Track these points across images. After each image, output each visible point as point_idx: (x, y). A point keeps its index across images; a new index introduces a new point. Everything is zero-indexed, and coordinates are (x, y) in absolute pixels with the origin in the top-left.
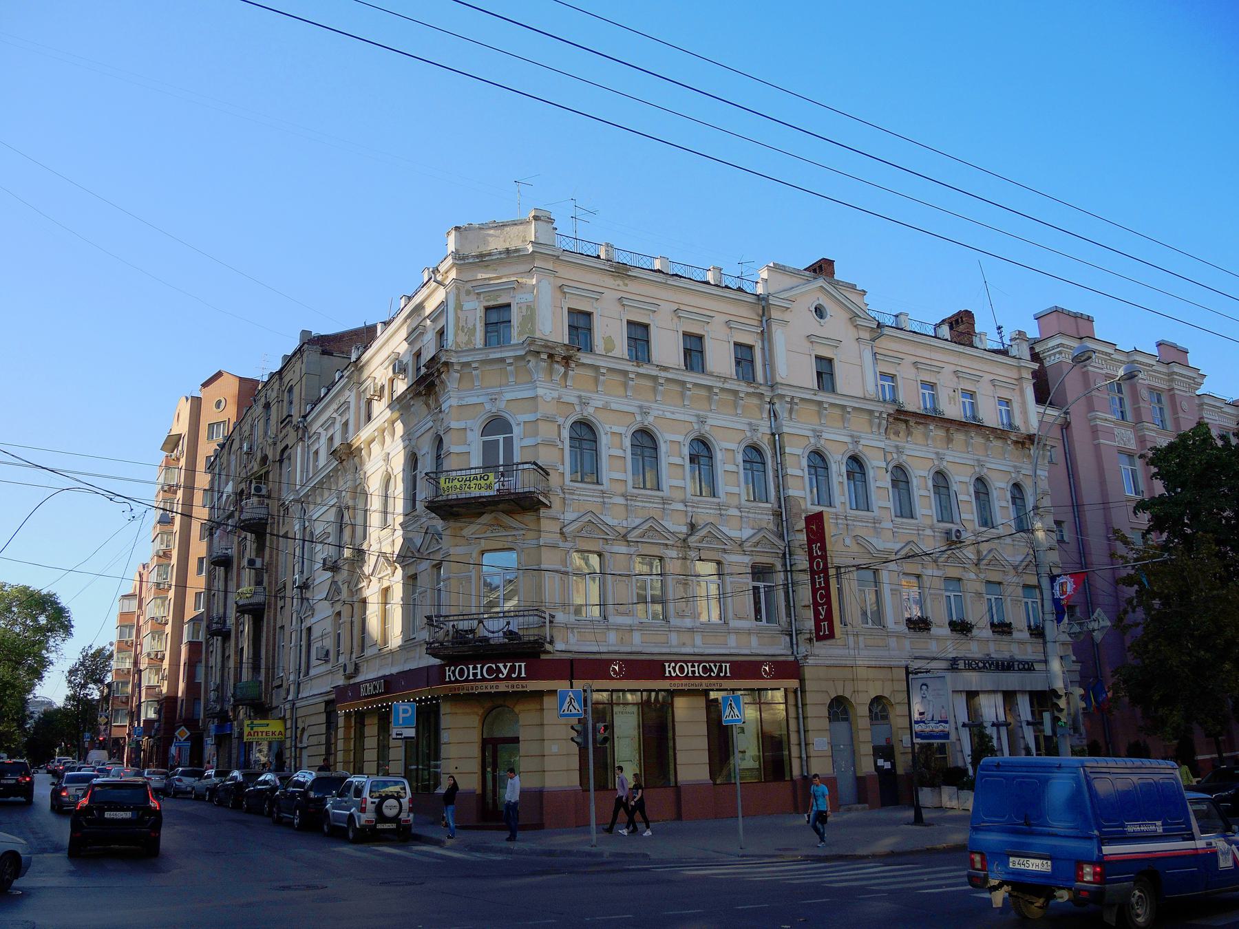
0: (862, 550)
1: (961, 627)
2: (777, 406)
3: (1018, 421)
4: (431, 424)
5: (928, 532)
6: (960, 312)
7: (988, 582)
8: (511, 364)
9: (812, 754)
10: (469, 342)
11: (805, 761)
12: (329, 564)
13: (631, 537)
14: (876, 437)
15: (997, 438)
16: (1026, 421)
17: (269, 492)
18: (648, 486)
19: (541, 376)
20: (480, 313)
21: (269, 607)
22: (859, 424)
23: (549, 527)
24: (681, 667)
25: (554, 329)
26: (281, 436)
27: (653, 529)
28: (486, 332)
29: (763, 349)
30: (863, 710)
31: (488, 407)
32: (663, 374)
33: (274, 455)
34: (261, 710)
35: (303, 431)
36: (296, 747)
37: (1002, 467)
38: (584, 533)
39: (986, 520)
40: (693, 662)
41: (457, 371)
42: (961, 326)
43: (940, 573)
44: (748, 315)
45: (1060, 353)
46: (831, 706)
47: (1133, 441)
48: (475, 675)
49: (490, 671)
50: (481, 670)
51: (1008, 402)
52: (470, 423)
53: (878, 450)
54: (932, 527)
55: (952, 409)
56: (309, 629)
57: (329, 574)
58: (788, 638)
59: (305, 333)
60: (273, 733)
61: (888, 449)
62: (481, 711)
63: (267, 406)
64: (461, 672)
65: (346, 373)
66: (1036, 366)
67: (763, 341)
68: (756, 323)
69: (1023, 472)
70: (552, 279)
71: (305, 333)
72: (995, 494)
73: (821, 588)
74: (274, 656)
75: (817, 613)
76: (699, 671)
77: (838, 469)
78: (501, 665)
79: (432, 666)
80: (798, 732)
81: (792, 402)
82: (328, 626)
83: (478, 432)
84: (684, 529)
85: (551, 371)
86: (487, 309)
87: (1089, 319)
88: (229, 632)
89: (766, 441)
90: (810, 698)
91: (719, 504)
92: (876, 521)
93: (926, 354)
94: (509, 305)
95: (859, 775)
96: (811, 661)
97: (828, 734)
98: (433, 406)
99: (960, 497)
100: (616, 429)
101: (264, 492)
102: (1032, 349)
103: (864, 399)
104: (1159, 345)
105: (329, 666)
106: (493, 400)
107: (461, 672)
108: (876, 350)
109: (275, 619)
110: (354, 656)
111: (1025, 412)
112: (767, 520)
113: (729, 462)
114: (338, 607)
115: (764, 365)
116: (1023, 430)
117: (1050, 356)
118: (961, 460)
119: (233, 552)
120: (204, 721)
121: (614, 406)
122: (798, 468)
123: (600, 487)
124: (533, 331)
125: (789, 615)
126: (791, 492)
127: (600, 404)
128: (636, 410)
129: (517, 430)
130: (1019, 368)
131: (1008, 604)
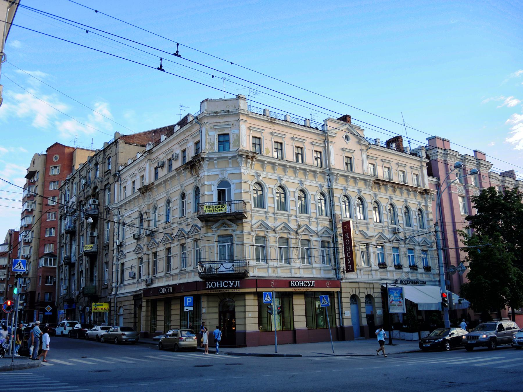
0: (362, 236)
1: (398, 267)
4: (193, 181)
5: (386, 228)
8: (230, 159)
9: (344, 317)
10: (212, 149)
13: (277, 230)
19: (243, 165)
20: (216, 137)
22: (361, 184)
24: (297, 283)
25: (246, 145)
26: (104, 179)
27: (286, 227)
28: (219, 145)
29: (325, 153)
30: (363, 300)
31: (220, 176)
32: (289, 164)
34: (96, 298)
36: (116, 315)
37: (414, 202)
38: (282, 231)
39: (409, 224)
40: (301, 281)
42: (395, 142)
43: (391, 245)
44: (319, 140)
46: (351, 298)
48: (219, 286)
49: (226, 284)
50: (222, 284)
52: (212, 182)
53: (368, 194)
54: (388, 227)
55: (397, 179)
56: (123, 264)
57: (135, 241)
60: (105, 309)
62: (219, 300)
64: (214, 285)
66: (428, 161)
72: (412, 213)
73: (349, 251)
74: (102, 275)
75: (347, 261)
76: (303, 284)
78: (230, 282)
79: (198, 281)
80: (339, 308)
81: (337, 176)
82: (135, 263)
83: (216, 187)
85: (246, 163)
86: (219, 135)
87: (448, 141)
89: (326, 191)
90: (343, 295)
94: (228, 134)
96: (344, 280)
98: (194, 174)
99: (399, 214)
100: (270, 186)
101: (97, 203)
102: (426, 153)
103: (363, 174)
105: (135, 280)
106: (223, 174)
107: (214, 285)
109: (102, 259)
110: (150, 276)
112: (327, 224)
114: (140, 256)
115: (326, 160)
118: (399, 200)
121: (270, 177)
123: (265, 210)
124: (239, 146)
125: (335, 262)
127: (264, 176)
130: (421, 162)
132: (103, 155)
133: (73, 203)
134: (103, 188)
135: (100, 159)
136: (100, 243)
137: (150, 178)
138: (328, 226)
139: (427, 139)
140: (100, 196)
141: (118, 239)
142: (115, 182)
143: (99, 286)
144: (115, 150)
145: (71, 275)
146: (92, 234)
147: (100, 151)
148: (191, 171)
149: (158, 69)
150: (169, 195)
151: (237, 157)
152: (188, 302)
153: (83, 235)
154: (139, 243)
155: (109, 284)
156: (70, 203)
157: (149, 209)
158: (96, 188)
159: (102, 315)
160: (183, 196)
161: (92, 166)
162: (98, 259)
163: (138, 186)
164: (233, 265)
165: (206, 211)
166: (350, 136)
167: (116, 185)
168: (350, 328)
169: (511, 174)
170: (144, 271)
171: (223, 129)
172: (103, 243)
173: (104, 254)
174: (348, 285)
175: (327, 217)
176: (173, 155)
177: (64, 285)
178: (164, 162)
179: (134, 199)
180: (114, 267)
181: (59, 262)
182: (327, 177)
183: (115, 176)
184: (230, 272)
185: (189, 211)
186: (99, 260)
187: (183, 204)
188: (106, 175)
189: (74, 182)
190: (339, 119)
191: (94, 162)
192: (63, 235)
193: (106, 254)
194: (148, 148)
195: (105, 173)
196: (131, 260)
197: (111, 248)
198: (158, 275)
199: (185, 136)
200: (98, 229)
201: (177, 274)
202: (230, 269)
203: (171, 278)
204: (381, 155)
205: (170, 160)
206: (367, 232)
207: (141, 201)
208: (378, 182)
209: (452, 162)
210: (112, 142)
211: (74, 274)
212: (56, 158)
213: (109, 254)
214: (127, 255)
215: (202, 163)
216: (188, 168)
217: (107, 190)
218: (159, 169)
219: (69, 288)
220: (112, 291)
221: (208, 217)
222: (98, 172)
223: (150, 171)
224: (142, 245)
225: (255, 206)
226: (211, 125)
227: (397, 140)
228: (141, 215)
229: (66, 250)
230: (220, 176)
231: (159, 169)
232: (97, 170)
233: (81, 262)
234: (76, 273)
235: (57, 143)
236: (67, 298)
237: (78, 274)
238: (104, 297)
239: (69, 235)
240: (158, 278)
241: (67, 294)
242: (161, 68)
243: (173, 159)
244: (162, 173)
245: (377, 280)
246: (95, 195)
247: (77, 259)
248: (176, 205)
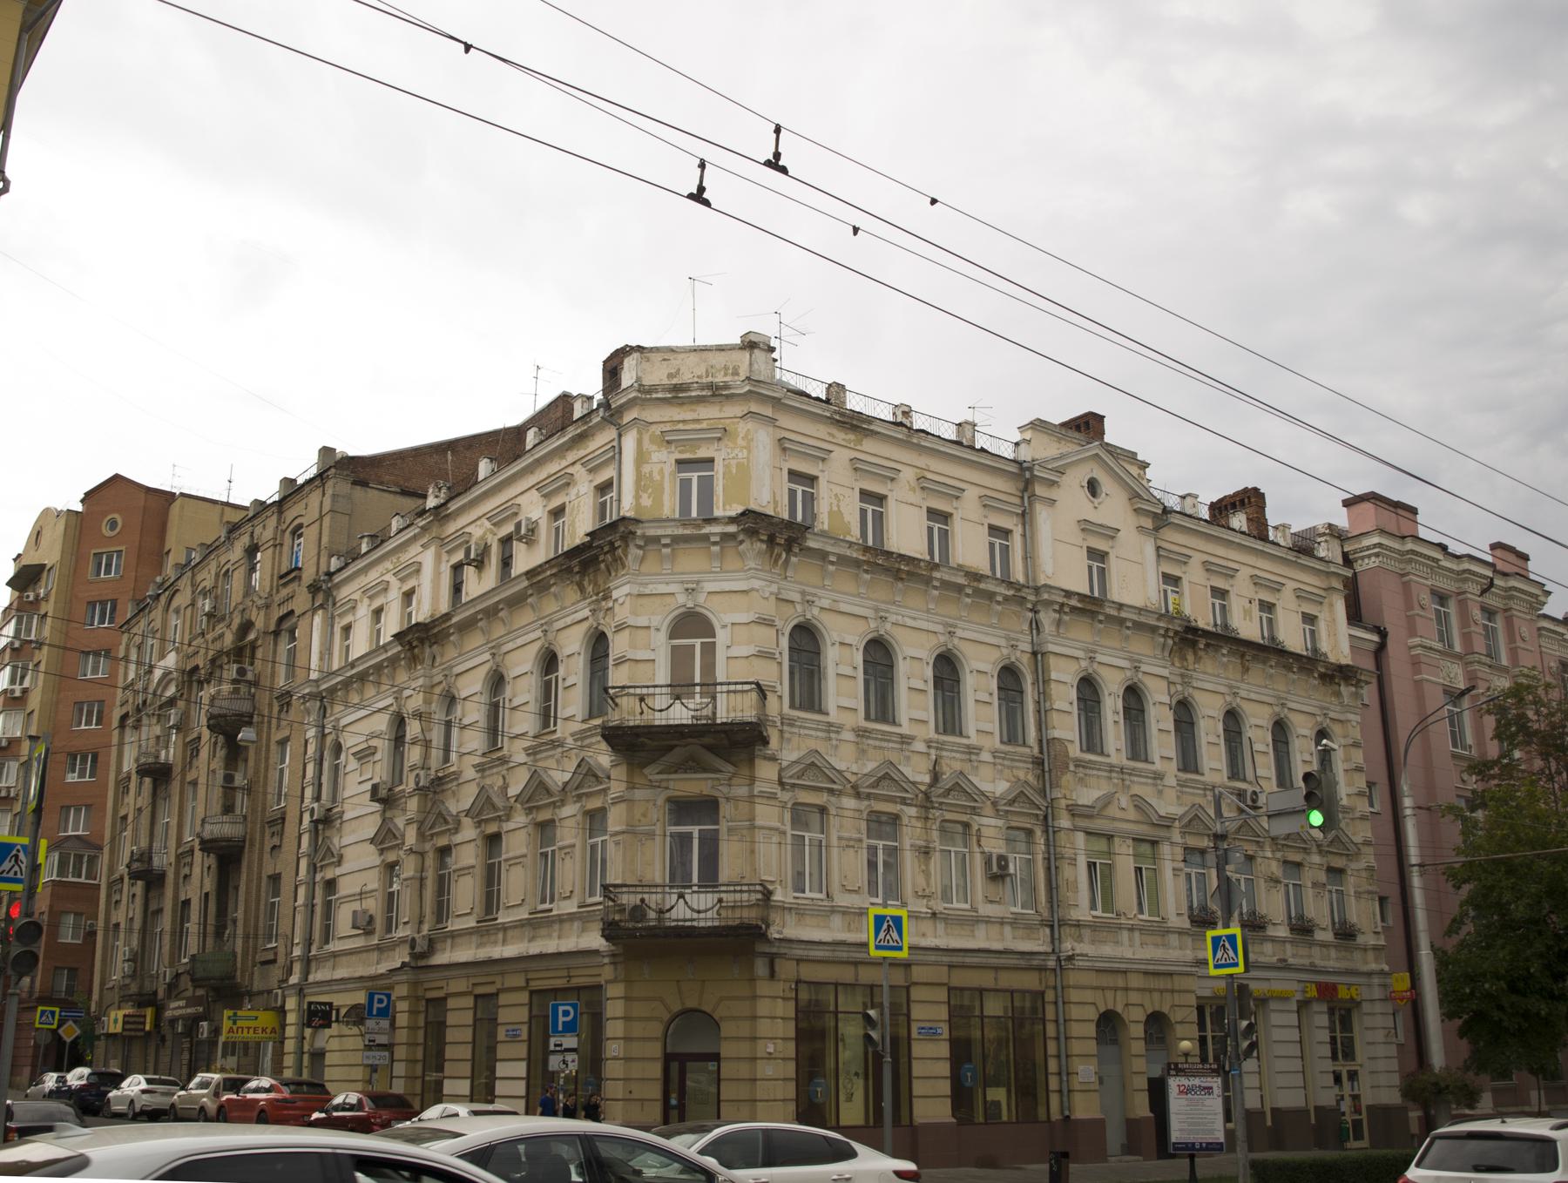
2: (1042, 615)
3: (1325, 646)
4: (586, 612)
6: (1246, 490)
7: (1285, 862)
11: (1066, 1093)
12: (383, 793)
14: (1161, 662)
15: (1301, 669)
16: (1335, 646)
18: (873, 716)
20: (670, 467)
21: (252, 845)
23: (766, 772)
26: (277, 599)
29: (1024, 535)
30: (1137, 1030)
33: (266, 625)
37: (1305, 706)
41: (639, 547)
45: (1377, 555)
51: (1006, 533)
55: (1248, 627)
58: (1048, 930)
59: (326, 452)
61: (1173, 678)
63: (252, 550)
65: (421, 522)
66: (1349, 573)
67: (1024, 525)
70: (771, 429)
71: (326, 452)
84: (927, 779)
88: (162, 876)
91: (968, 746)
92: (1158, 776)
94: (712, 460)
97: (1095, 1060)
98: (590, 589)
99: (1257, 747)
101: (250, 676)
104: (1347, 503)
108: (1160, 543)
111: (1333, 634)
116: (1332, 659)
117: (1363, 558)
118: (1260, 698)
119: (171, 754)
122: (1065, 697)
125: (1050, 900)
126: (1056, 734)
128: (796, 597)
129: (722, 637)
131: (1309, 893)
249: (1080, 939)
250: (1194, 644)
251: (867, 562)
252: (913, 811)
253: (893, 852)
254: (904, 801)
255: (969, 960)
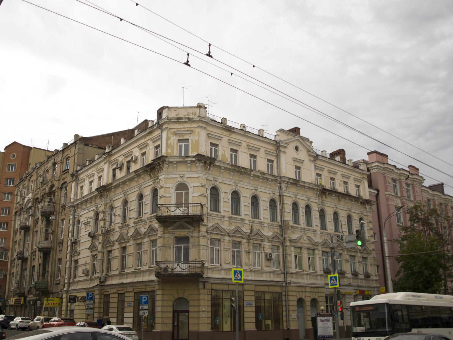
3: (362, 194)
4: (152, 183)
6: (340, 150)
8: (189, 163)
11: (288, 321)
12: (92, 235)
15: (355, 201)
17: (56, 201)
18: (234, 213)
20: (176, 141)
23: (203, 229)
26: (62, 178)
27: (238, 231)
30: (308, 304)
33: (58, 185)
35: (75, 176)
37: (356, 211)
41: (167, 164)
44: (272, 148)
45: (377, 168)
47: (400, 203)
55: (340, 189)
56: (76, 261)
57: (90, 239)
58: (283, 275)
59: (76, 136)
61: (319, 203)
63: (54, 164)
67: (277, 159)
68: (275, 152)
69: (364, 214)
77: (302, 211)
82: (89, 260)
84: (249, 231)
88: (27, 259)
91: (261, 222)
93: (333, 167)
94: (188, 140)
95: (307, 328)
97: (296, 312)
98: (153, 176)
101: (53, 201)
111: (364, 191)
113: (264, 206)
114: (94, 253)
116: (364, 198)
120: (8, 296)
121: (226, 182)
122: (288, 208)
126: (286, 219)
127: (220, 181)
129: (191, 190)
131: (357, 265)
132: (61, 154)
133: (28, 200)
134: (60, 186)
135: (59, 158)
136: (54, 239)
137: (108, 178)
138: (279, 231)
139: (368, 154)
140: (56, 194)
141: (73, 236)
142: (72, 182)
143: (51, 281)
144: (74, 151)
145: (23, 270)
146: (47, 230)
147: (57, 151)
148: (150, 173)
149: (185, 63)
150: (126, 196)
151: (196, 162)
152: (143, 300)
153: (37, 232)
154: (93, 241)
155: (62, 280)
156: (26, 199)
157: (105, 208)
158: (53, 186)
159: (52, 310)
160: (141, 197)
161: (50, 164)
162: (51, 255)
163: (95, 186)
164: (190, 266)
165: (163, 212)
166: (301, 148)
167: (73, 184)
168: (297, 331)
169: (439, 188)
170: (98, 269)
171: (183, 135)
172: (57, 239)
173: (58, 251)
174: (295, 289)
175: (277, 223)
176: (132, 158)
177: (15, 280)
178: (123, 164)
179: (91, 198)
180: (68, 263)
181: (12, 257)
182: (279, 185)
183: (72, 175)
184: (186, 273)
185: (146, 212)
186: (53, 256)
187: (140, 206)
188: (64, 174)
189: (31, 180)
190: (290, 131)
191: (52, 161)
192: (17, 230)
193: (60, 250)
194: (107, 151)
195: (63, 172)
196: (84, 256)
197: (65, 245)
198: (112, 273)
199: (146, 140)
200: (53, 226)
201: (132, 273)
202: (186, 270)
203: (126, 276)
204: (327, 166)
205: (129, 162)
206: (313, 238)
207: (98, 201)
208: (323, 192)
209: (390, 176)
210: (71, 143)
211: (26, 269)
212: (14, 156)
213: (63, 251)
214: (81, 252)
215: (161, 165)
216: (147, 171)
217: (64, 189)
218: (118, 171)
219: (19, 283)
220: (64, 287)
221: (166, 218)
222: (56, 171)
223: (108, 171)
224: (97, 243)
225: (211, 210)
226: (173, 130)
227: (341, 153)
228: (97, 214)
229: (19, 245)
230: (213, 182)
231: (118, 171)
232: (55, 169)
233: (34, 257)
234: (28, 267)
235: (15, 143)
236: (18, 291)
237: (30, 269)
238: (55, 293)
239: (23, 231)
240: (112, 276)
241: (18, 288)
242: (187, 63)
243: (132, 162)
244: (120, 175)
245: (322, 284)
246: (51, 193)
247: (30, 254)
248: (133, 205)
249: (292, 277)
250: (325, 193)
251: (233, 169)
252: (245, 241)
253: (239, 252)
254: (242, 238)
255: (261, 283)
